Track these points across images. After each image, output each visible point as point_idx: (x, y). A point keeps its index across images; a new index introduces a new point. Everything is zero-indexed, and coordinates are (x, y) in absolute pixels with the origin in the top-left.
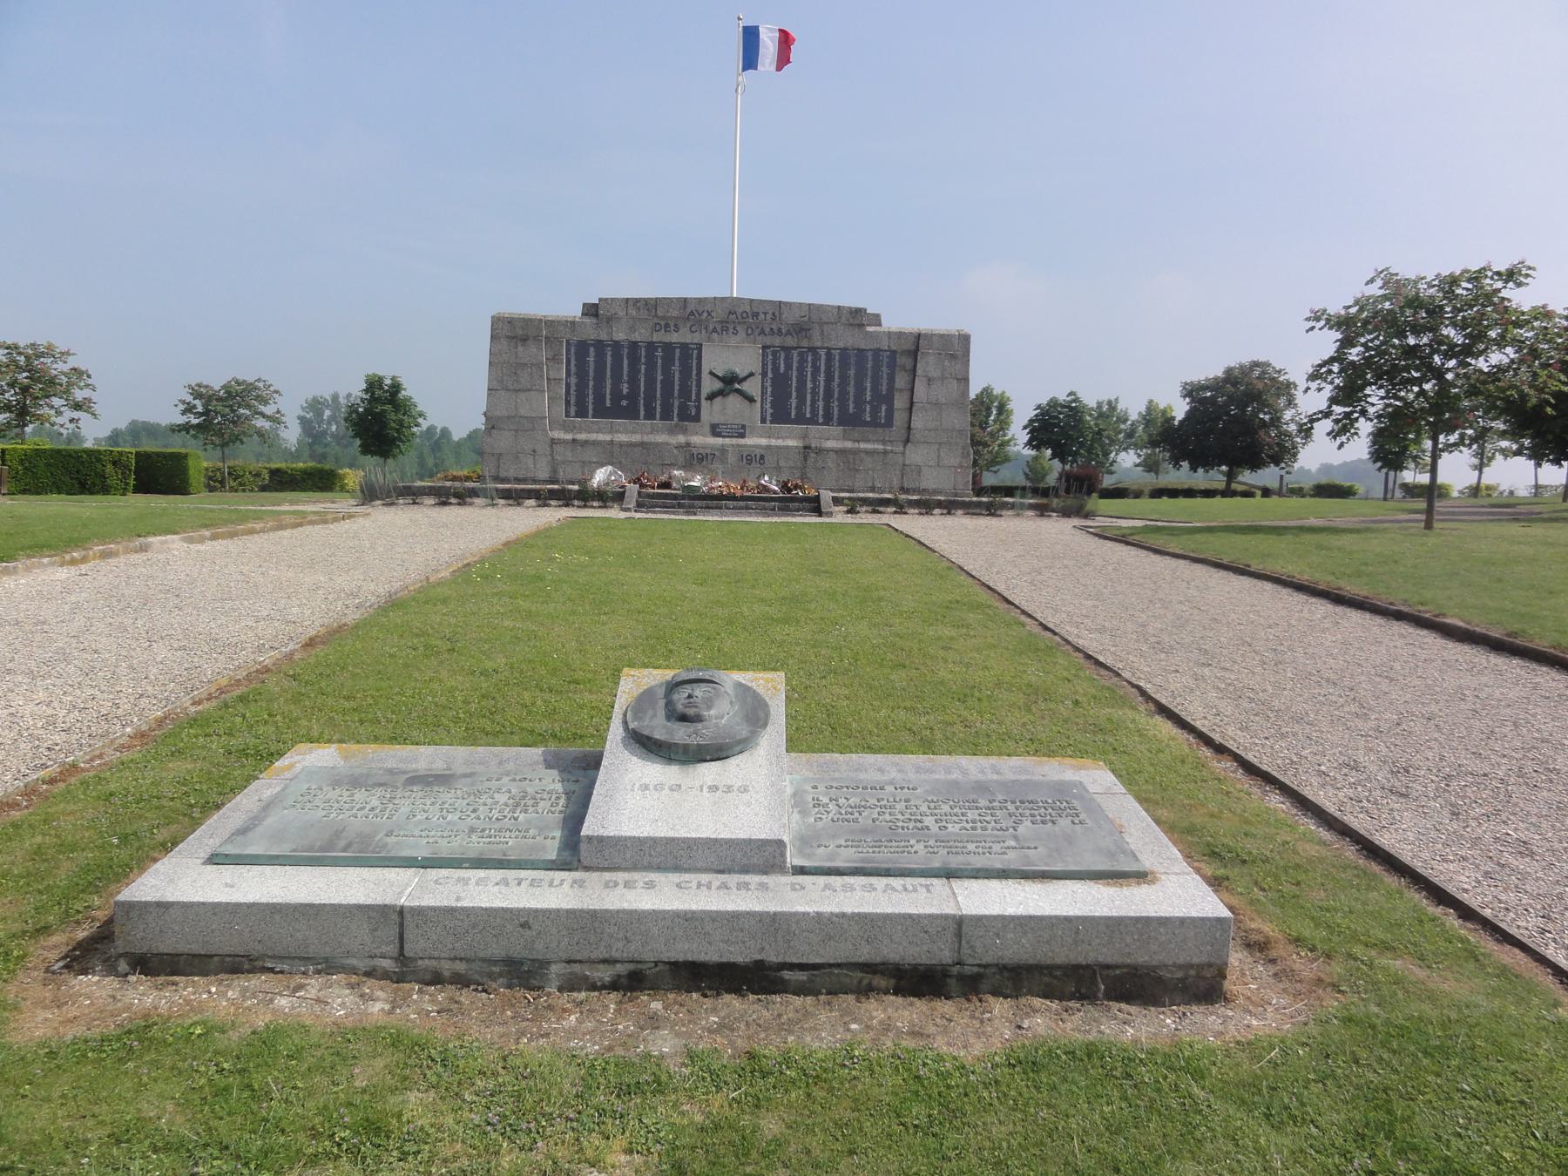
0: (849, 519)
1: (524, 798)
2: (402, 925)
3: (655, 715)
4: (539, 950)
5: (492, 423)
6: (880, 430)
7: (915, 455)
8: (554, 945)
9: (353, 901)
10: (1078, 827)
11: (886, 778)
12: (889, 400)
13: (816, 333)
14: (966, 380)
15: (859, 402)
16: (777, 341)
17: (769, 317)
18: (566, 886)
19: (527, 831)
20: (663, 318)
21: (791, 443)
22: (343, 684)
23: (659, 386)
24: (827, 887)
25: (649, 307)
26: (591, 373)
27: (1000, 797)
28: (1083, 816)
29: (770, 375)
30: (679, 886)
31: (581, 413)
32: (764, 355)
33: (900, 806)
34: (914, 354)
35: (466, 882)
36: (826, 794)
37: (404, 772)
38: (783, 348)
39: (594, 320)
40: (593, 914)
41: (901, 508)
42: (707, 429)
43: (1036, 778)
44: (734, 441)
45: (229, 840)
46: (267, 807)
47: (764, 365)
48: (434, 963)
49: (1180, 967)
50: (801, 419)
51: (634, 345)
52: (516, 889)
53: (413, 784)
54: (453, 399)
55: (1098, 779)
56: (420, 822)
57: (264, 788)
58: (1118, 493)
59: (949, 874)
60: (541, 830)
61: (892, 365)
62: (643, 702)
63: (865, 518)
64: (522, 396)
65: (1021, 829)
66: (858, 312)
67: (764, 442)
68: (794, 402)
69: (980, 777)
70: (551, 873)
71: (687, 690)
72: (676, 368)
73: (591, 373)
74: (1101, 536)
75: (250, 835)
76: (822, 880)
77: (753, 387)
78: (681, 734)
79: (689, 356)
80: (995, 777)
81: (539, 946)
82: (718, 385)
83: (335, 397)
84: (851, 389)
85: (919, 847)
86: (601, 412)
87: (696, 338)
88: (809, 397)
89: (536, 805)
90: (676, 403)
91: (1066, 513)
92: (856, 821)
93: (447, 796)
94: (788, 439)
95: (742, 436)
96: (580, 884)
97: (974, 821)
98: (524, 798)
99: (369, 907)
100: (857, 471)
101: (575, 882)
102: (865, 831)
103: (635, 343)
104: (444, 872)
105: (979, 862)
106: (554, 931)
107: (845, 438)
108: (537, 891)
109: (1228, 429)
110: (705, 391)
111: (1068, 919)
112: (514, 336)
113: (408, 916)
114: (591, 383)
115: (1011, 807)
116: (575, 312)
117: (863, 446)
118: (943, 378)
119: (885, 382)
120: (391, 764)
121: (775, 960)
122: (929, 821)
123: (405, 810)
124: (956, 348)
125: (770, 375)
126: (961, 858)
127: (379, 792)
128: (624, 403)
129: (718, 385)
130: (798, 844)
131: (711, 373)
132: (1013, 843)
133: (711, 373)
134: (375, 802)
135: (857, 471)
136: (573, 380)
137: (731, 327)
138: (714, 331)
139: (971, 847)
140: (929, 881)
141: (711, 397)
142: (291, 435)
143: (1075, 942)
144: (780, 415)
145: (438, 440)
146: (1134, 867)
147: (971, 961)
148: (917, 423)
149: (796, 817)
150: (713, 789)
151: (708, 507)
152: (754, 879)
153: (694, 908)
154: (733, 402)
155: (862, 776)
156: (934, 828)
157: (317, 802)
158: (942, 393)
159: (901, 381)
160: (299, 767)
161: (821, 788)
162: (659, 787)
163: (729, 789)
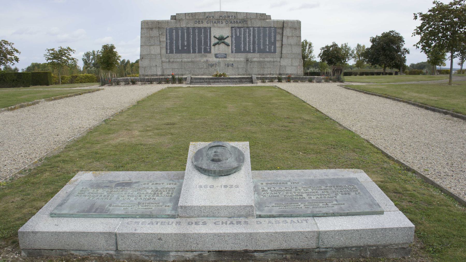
0: (263, 84)
1: (157, 191)
2: (116, 239)
3: (202, 159)
4: (165, 248)
5: (142, 57)
6: (272, 54)
7: (284, 62)
8: (171, 246)
9: (99, 231)
10: (358, 195)
11: (287, 179)
12: (274, 44)
13: (249, 22)
14: (300, 37)
15: (265, 45)
16: (236, 25)
17: (233, 17)
18: (174, 225)
19: (159, 203)
20: (197, 19)
21: (242, 59)
22: (95, 150)
23: (197, 42)
24: (269, 222)
25: (193, 16)
26: (174, 39)
27: (329, 185)
28: (359, 191)
29: (234, 37)
30: (215, 223)
31: (171, 52)
32: (232, 30)
33: (294, 190)
34: (283, 28)
35: (138, 223)
36: (266, 186)
37: (115, 182)
38: (238, 27)
39: (175, 21)
40: (184, 235)
41: (280, 80)
42: (214, 56)
43: (340, 177)
44: (223, 59)
45: (56, 208)
46: (69, 196)
47: (232, 33)
48: (129, 252)
49: (396, 245)
50: (245, 51)
51: (188, 28)
52: (156, 226)
53: (118, 186)
54: (129, 50)
55: (361, 176)
56: (121, 201)
57: (68, 188)
58: (349, 74)
59: (314, 216)
60: (164, 203)
61: (275, 32)
62: (199, 154)
63: (268, 84)
64: (152, 47)
65: (338, 197)
66: (263, 15)
67: (233, 59)
68: (242, 46)
69: (321, 178)
70: (168, 219)
71: (214, 150)
72: (203, 35)
73: (174, 39)
74: (347, 88)
75: (63, 206)
76: (267, 220)
77: (228, 41)
78: (214, 167)
79: (207, 31)
80: (326, 177)
81: (165, 246)
82: (217, 41)
83: (94, 52)
84: (262, 41)
85: (302, 205)
86: (178, 51)
87: (209, 25)
88: (247, 43)
89: (161, 193)
90: (203, 47)
91: (334, 81)
92: (278, 196)
93: (130, 191)
94: (241, 57)
95: (226, 57)
96: (179, 223)
97: (321, 195)
98: (157, 191)
99: (104, 233)
100: (264, 68)
101: (177, 223)
102: (282, 200)
103: (188, 28)
104: (130, 220)
105: (325, 210)
106: (170, 241)
107: (260, 57)
108: (164, 227)
109: (385, 52)
110: (212, 43)
111: (357, 230)
112: (149, 28)
113: (118, 236)
114: (174, 42)
115: (333, 189)
116: (169, 18)
117: (266, 59)
118: (292, 36)
119: (273, 38)
120: (110, 179)
121: (251, 249)
122: (305, 195)
123: (116, 196)
124: (296, 26)
125: (234, 37)
126: (317, 210)
127: (107, 189)
128: (185, 48)
129: (217, 41)
130: (258, 206)
131: (214, 37)
132: (335, 203)
133: (214, 37)
134: (105, 194)
135: (264, 68)
136: (168, 41)
137: (221, 21)
138: (215, 22)
139: (321, 205)
140: (306, 218)
141: (215, 45)
142: (81, 65)
143: (360, 238)
144: (238, 50)
145: (126, 64)
146: (379, 210)
147: (323, 247)
148: (284, 52)
149: (256, 195)
150: (226, 186)
151: (214, 82)
152: (242, 220)
153: (221, 232)
154: (222, 46)
155: (279, 179)
156: (307, 198)
157: (86, 194)
158: (293, 41)
159: (278, 37)
160: (79, 180)
161: (264, 184)
162: (206, 187)
163: (231, 186)
